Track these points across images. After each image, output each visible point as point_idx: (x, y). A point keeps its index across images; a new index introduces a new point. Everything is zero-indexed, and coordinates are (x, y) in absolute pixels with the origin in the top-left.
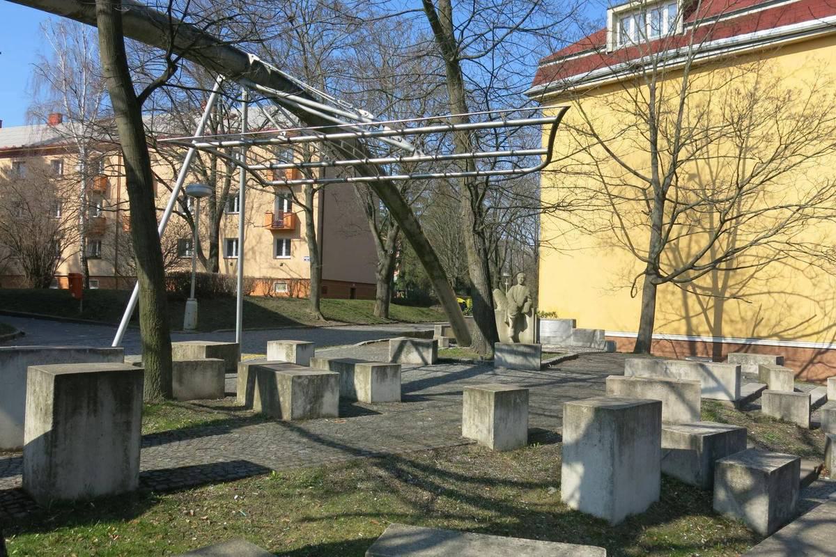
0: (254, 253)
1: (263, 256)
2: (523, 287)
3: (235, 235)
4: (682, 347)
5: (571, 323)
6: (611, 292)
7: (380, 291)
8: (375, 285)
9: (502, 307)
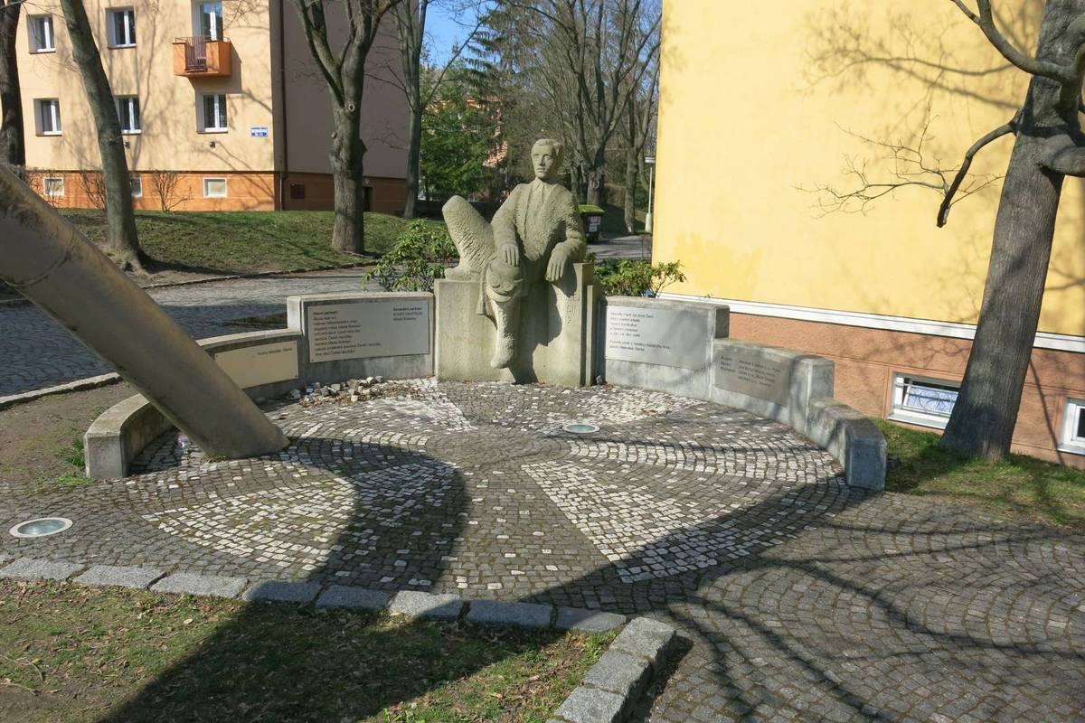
0: (164, 122)
1: (180, 127)
2: (550, 190)
3: (129, 89)
4: (1064, 370)
5: (711, 320)
6: (855, 203)
7: (342, 195)
8: (331, 176)
9: (475, 257)
